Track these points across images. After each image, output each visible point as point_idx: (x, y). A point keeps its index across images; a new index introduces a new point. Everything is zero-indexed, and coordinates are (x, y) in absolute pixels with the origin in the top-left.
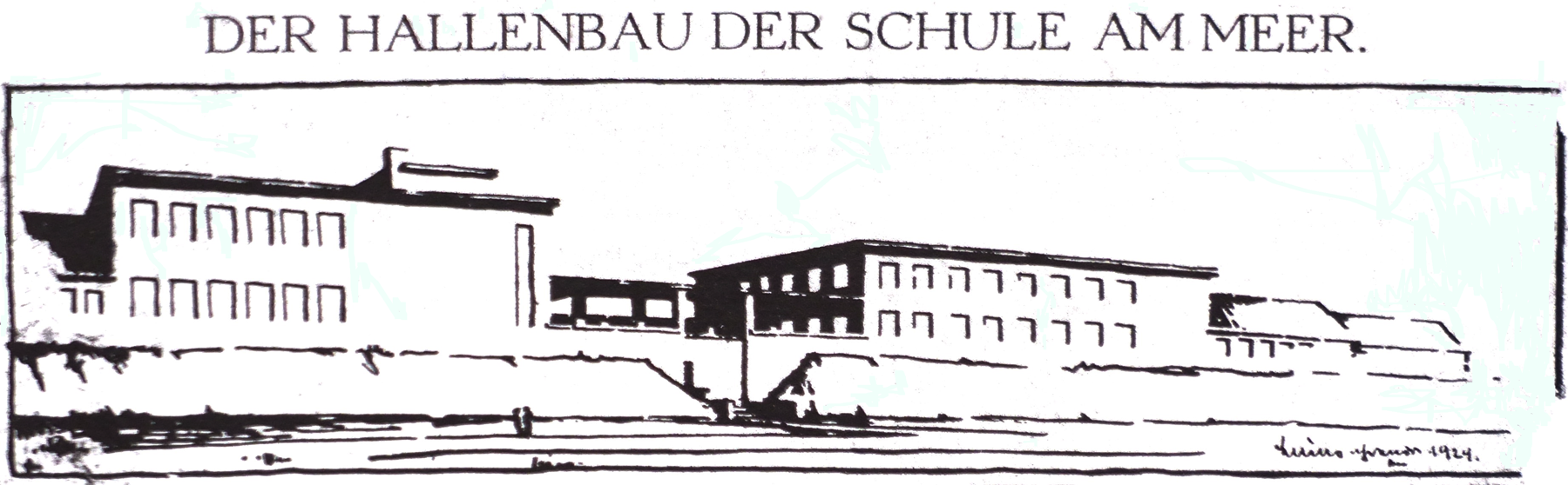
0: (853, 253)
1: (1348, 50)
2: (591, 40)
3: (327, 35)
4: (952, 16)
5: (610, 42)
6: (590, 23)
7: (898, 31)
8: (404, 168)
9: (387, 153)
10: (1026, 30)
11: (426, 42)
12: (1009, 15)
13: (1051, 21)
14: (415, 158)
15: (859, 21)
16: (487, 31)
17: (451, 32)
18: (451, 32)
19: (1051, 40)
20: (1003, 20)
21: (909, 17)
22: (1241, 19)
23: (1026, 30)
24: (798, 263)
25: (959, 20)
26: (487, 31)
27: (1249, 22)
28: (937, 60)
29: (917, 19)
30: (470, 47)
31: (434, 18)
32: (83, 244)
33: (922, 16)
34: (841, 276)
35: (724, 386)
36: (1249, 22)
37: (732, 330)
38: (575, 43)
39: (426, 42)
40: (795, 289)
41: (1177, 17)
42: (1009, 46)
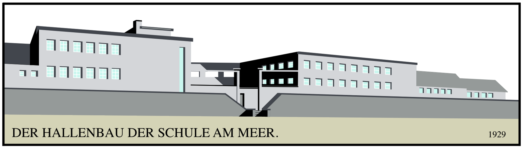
0: (294, 57)
1: (273, 136)
2: (100, 135)
3: (40, 133)
4: (182, 129)
5: (105, 135)
6: (100, 131)
7: (171, 133)
8: (141, 27)
9: (135, 23)
10: (200, 132)
11: (61, 135)
12: (196, 129)
13: (206, 130)
14: (143, 24)
15: (161, 130)
16: (76, 132)
17: (67, 132)
18: (67, 132)
19: (206, 135)
20: (194, 130)
21: (173, 129)
22: (247, 129)
23: (200, 132)
24: (275, 60)
25: (184, 131)
26: (76, 132)
27: (249, 131)
28: (179, 140)
29: (175, 130)
30: (72, 136)
31: (63, 129)
32: (31, 53)
33: (176, 129)
34: (291, 65)
35: (251, 104)
36: (249, 131)
37: (255, 85)
38: (96, 135)
39: (61, 135)
40: (275, 69)
41: (232, 129)
42: (196, 136)
